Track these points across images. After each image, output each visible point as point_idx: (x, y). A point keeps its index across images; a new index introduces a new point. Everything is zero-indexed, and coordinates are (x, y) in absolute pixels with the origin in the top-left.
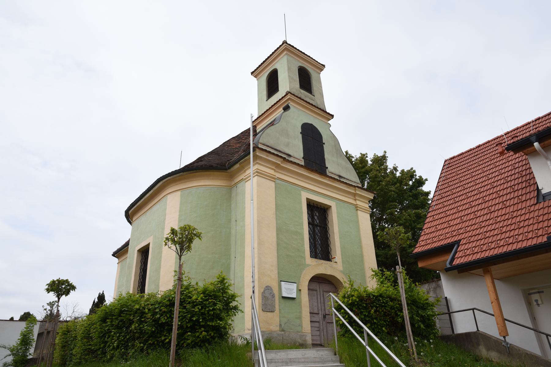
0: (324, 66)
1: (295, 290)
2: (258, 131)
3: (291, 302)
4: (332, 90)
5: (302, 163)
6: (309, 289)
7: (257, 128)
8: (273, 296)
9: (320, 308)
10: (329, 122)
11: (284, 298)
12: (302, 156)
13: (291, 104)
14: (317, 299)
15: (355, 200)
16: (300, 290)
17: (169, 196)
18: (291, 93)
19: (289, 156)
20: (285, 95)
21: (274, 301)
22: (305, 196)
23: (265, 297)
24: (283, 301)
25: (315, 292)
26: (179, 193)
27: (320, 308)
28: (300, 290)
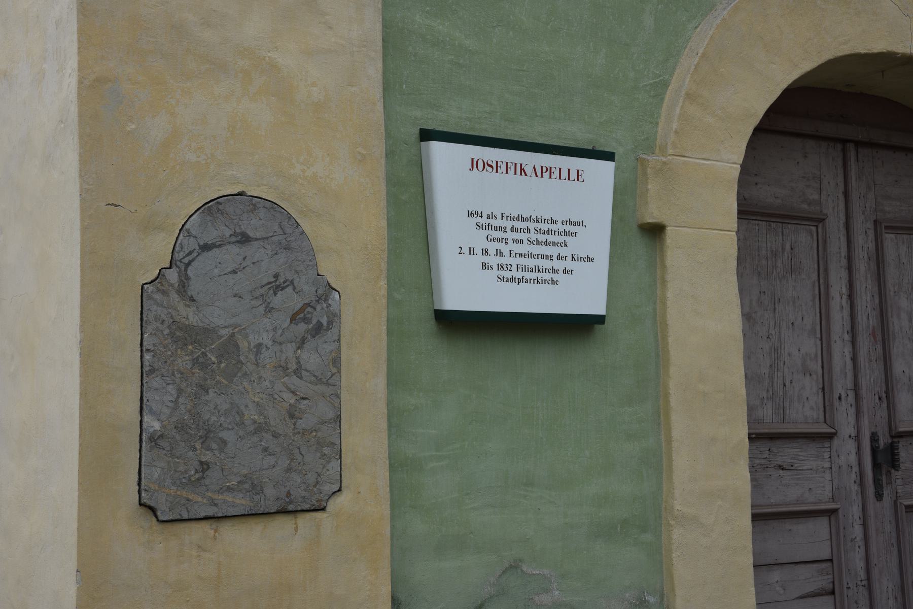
1: (596, 238)
3: (543, 361)
8: (316, 317)
16: (655, 232)
21: (330, 377)
23: (187, 336)
24: (444, 361)
25: (803, 238)
28: (655, 232)
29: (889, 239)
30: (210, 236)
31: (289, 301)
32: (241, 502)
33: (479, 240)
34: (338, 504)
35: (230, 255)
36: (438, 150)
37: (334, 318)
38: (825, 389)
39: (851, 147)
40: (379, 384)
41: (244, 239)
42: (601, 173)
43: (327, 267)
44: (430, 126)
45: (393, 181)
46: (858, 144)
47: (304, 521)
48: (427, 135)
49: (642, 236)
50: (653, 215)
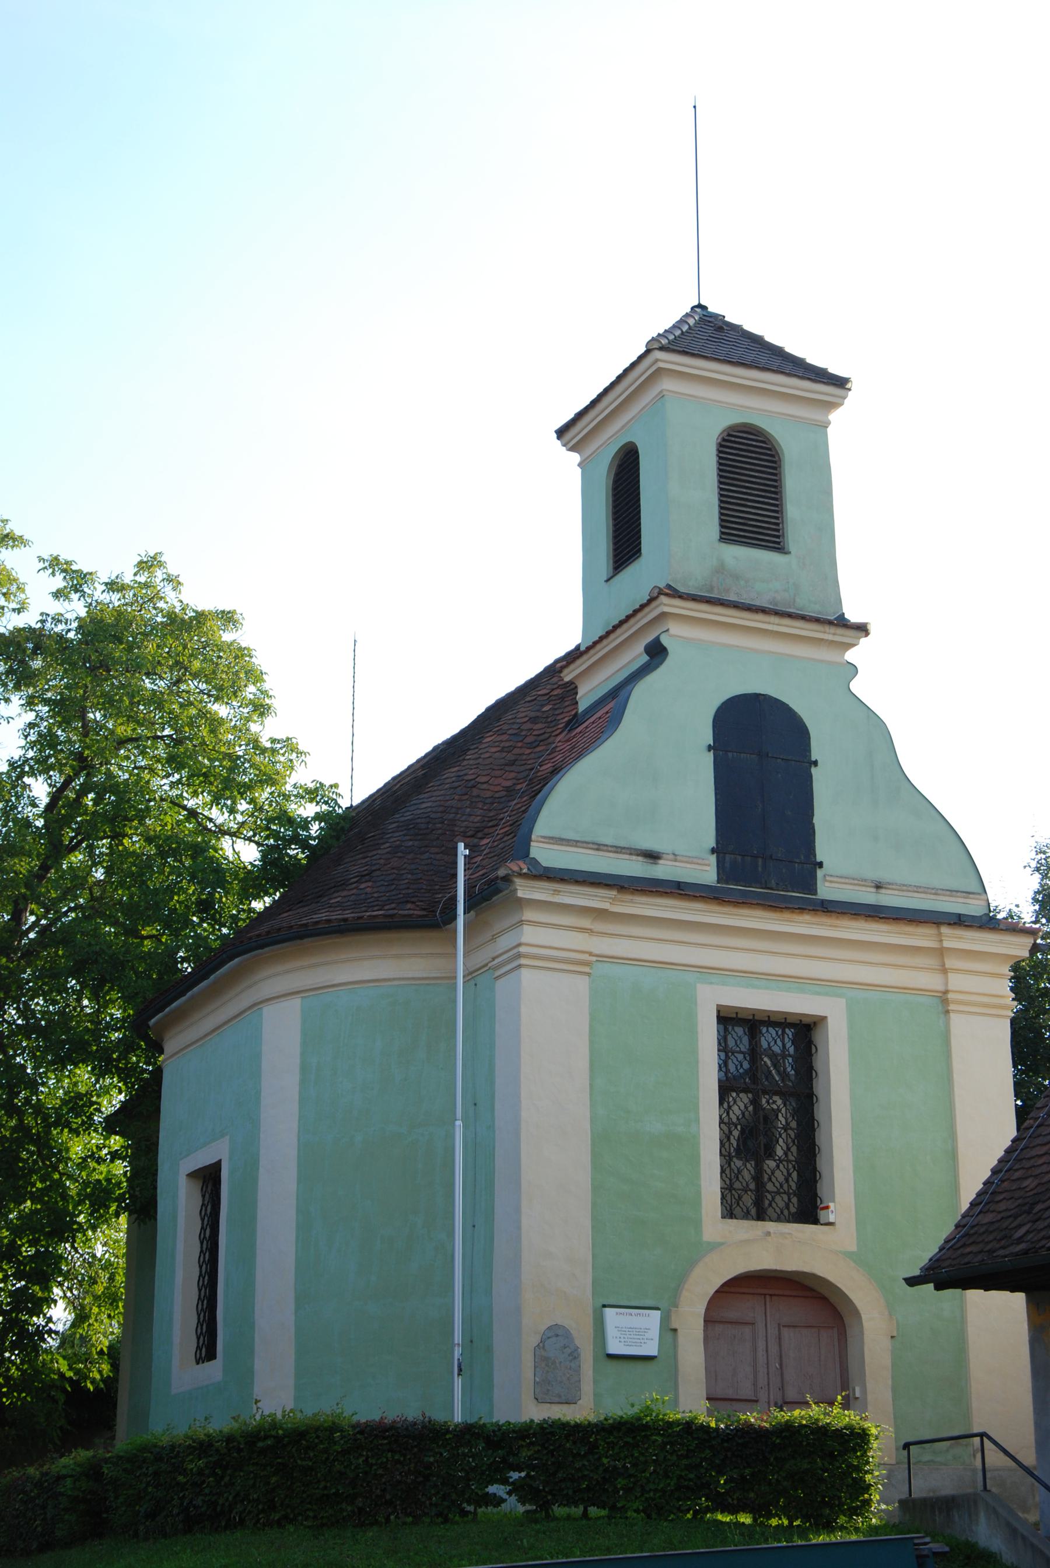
0: (841, 383)
1: (655, 1332)
2: (582, 707)
3: (640, 1366)
4: (879, 508)
5: (707, 873)
6: (709, 1320)
7: (581, 692)
8: (574, 1355)
9: (762, 1382)
10: (850, 656)
11: (611, 1357)
12: (710, 839)
13: (676, 636)
14: (755, 1350)
15: (944, 971)
16: (675, 1330)
17: (267, 1010)
18: (673, 593)
19: (652, 856)
20: (650, 601)
21: (578, 1370)
22: (711, 998)
23: (546, 1359)
24: (613, 1366)
25: (747, 1330)
26: (296, 1002)
27: (762, 1382)
28: (675, 1330)
29: (785, 1332)
30: (550, 1335)
31: (568, 1351)
32: (557, 1400)
33: (619, 1335)
34: (580, 1402)
35: (554, 1339)
36: (607, 1310)
37: (579, 1355)
38: (755, 1384)
39: (768, 1297)
40: (591, 1373)
41: (557, 1336)
42: (657, 1314)
43: (577, 1342)
44: (606, 1303)
45: (595, 1319)
46: (771, 1295)
47: (573, 1406)
48: (604, 1306)
49: (669, 1331)
50: (674, 1327)
